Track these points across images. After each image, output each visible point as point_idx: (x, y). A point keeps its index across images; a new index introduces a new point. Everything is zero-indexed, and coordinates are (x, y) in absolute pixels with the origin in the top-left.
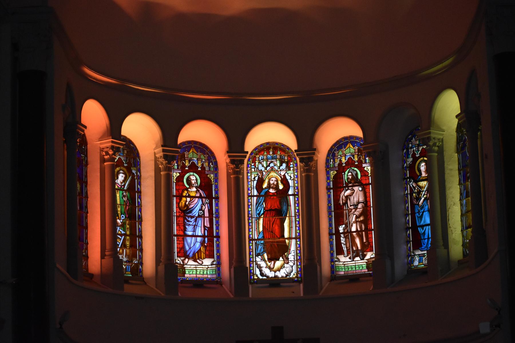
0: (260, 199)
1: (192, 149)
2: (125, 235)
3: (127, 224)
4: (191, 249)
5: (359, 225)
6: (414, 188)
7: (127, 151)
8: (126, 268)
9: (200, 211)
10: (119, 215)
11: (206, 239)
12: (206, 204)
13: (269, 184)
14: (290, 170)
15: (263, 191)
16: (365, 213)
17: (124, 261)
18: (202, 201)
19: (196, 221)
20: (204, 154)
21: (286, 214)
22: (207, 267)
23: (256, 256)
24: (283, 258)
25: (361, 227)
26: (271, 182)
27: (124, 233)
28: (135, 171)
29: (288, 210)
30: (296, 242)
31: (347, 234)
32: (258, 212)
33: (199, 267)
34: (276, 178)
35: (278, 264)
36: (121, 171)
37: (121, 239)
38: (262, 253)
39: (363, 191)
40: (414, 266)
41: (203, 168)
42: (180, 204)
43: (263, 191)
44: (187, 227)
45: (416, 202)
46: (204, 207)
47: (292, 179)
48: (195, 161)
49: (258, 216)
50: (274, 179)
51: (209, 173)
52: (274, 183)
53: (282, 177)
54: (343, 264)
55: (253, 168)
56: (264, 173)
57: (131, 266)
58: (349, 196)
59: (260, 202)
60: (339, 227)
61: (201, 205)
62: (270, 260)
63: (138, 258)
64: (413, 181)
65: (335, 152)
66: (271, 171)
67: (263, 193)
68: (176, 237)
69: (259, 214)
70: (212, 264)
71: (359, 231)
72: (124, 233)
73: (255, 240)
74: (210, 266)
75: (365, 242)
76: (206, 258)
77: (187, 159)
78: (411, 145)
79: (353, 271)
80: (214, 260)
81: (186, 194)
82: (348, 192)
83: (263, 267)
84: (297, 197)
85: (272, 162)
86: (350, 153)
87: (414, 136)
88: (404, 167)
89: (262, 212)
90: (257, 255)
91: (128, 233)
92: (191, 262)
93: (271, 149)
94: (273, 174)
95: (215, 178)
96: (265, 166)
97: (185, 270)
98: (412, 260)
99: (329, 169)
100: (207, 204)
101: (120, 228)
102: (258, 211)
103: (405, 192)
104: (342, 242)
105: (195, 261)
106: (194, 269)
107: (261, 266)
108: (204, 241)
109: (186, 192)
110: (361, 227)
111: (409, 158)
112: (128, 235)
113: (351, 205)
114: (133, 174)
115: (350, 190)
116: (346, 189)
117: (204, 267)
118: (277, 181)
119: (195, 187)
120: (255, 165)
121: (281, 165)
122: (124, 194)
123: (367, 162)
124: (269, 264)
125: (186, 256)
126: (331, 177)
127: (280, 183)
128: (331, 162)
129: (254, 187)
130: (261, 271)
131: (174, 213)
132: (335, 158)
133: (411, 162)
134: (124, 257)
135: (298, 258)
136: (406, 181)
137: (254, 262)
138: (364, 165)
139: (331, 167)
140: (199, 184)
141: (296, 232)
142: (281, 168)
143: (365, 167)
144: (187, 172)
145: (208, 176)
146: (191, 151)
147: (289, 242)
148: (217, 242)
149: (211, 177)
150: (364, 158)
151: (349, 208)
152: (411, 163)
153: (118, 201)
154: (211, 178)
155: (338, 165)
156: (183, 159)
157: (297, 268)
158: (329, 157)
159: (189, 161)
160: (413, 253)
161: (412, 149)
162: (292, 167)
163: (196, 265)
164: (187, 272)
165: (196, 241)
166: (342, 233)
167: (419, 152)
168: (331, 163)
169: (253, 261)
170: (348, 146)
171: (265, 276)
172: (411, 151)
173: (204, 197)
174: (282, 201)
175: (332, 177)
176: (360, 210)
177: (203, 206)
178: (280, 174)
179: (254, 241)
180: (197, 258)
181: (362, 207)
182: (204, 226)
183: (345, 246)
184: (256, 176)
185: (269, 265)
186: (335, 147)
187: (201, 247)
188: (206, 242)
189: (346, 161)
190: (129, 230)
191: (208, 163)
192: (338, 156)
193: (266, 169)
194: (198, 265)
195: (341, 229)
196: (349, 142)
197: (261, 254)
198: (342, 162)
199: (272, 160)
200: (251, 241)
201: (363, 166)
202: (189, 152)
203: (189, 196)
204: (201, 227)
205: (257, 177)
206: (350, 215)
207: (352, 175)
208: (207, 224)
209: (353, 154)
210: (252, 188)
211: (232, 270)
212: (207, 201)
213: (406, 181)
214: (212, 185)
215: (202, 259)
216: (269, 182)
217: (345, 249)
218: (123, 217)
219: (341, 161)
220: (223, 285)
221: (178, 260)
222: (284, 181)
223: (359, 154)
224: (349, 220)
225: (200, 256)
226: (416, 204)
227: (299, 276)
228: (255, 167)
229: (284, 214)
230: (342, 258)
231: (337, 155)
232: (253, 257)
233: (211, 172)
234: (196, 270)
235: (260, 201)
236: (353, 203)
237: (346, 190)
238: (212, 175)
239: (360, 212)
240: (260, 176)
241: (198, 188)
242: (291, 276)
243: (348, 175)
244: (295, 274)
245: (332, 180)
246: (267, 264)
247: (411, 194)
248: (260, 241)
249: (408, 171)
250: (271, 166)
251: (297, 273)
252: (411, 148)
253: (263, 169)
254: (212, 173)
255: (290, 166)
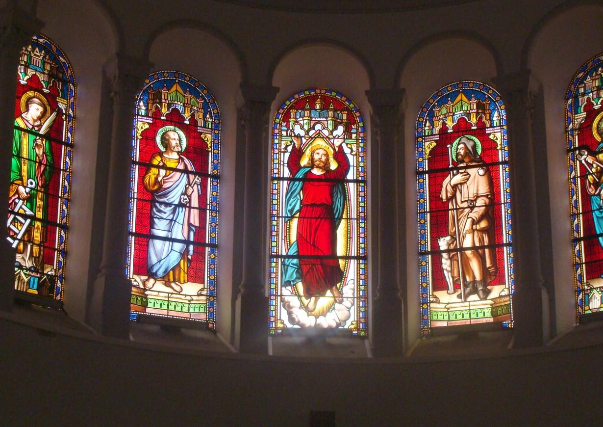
0: (294, 185)
1: (175, 86)
2: (33, 218)
3: (39, 199)
4: (162, 262)
5: (478, 236)
6: (591, 165)
7: (51, 67)
8: (29, 282)
9: (182, 196)
10: (25, 179)
11: (191, 248)
12: (196, 185)
13: (312, 160)
14: (351, 138)
15: (301, 170)
16: (492, 212)
17: (26, 267)
18: (188, 178)
19: (174, 212)
20: (196, 97)
21: (341, 213)
22: (189, 298)
23: (282, 286)
24: (332, 292)
25: (481, 240)
26: (316, 157)
27: (31, 213)
28: (64, 106)
29: (346, 206)
30: (359, 264)
31: (455, 253)
32: (290, 208)
33: (173, 298)
34: (325, 150)
35: (325, 300)
36: (36, 100)
37: (23, 224)
38: (293, 281)
39: (486, 176)
40: (590, 309)
41: (193, 119)
42: (147, 180)
43: (300, 171)
44: (156, 220)
45: (594, 191)
46: (190, 190)
47: (354, 153)
48: (179, 106)
49: (289, 215)
50: (321, 152)
51: (204, 132)
52: (321, 158)
53: (337, 149)
54: (445, 308)
55: (284, 130)
56: (304, 141)
57: (40, 278)
58: (459, 186)
59: (293, 189)
60: (439, 239)
61: (186, 185)
62: (309, 293)
63: (56, 266)
64: (586, 153)
65: (434, 110)
66: (317, 137)
67: (300, 175)
68: (133, 238)
69: (291, 211)
70: (199, 295)
71: (479, 248)
72: (31, 213)
73: (282, 256)
74: (194, 298)
75: (490, 268)
76: (188, 281)
77: (164, 102)
78: (583, 89)
79: (465, 321)
80: (204, 288)
81: (160, 162)
82: (458, 179)
83: (295, 307)
84: (363, 185)
85: (319, 122)
86: (462, 110)
87: (589, 73)
88: (569, 130)
89: (297, 208)
90: (288, 283)
91: (39, 215)
92: (160, 286)
93: (319, 100)
94: (319, 142)
95: (214, 142)
96: (306, 127)
97: (147, 299)
98: (585, 298)
99: (423, 139)
100: (198, 185)
101: (23, 204)
102: (290, 205)
103: (571, 174)
104: (444, 266)
105: (167, 284)
106: (165, 300)
107: (291, 304)
108: (187, 250)
109: (159, 158)
110: (481, 240)
111: (579, 112)
112: (39, 220)
113: (462, 200)
114: (60, 110)
115: (461, 175)
116: (453, 173)
117: (183, 297)
118: (327, 155)
119: (176, 152)
120: (288, 126)
121: (335, 128)
122: (39, 142)
123: (495, 125)
124: (306, 301)
125: (152, 275)
126: (425, 153)
127: (331, 159)
128: (425, 126)
129: (284, 163)
130: (290, 314)
131: (134, 193)
132: (434, 119)
133: (582, 120)
134: (27, 259)
135: (361, 294)
136: (573, 154)
137: (279, 298)
138: (488, 131)
139: (427, 134)
140: (184, 148)
141: (358, 247)
142: (335, 133)
143: (490, 134)
144: (165, 123)
145: (203, 136)
146: (174, 88)
147: (346, 263)
148: (210, 254)
149: (206, 139)
150: (488, 118)
151: (459, 206)
152: (583, 121)
153: (25, 153)
154: (208, 140)
155: (439, 132)
156: (158, 101)
157: (359, 311)
158: (423, 119)
159: (169, 105)
160: (587, 285)
161: (586, 97)
162: (354, 133)
163: (169, 293)
164: (150, 305)
165: (172, 249)
166: (444, 251)
167: (600, 101)
168: (427, 128)
169: (276, 296)
170: (459, 98)
171: (298, 323)
172: (583, 101)
173: (192, 173)
174: (334, 190)
175: (428, 152)
176: (480, 210)
177: (190, 187)
178: (333, 144)
179: (280, 259)
180: (171, 279)
181: (484, 205)
182: (190, 224)
183: (450, 274)
184: (289, 145)
185: (306, 304)
186: (434, 101)
187: (180, 261)
188: (191, 252)
189: (455, 124)
190: (41, 210)
191: (203, 113)
192: (439, 116)
193: (307, 132)
194: (172, 293)
195: (443, 243)
196: (461, 92)
197: (292, 283)
198: (447, 126)
199: (319, 119)
200: (275, 259)
201: (487, 132)
202: (169, 90)
203: (164, 167)
204: (183, 225)
205: (292, 146)
206: (460, 219)
207: (466, 147)
208: (195, 221)
209: (468, 112)
210: (281, 165)
211: (239, 303)
212: (198, 179)
213: (573, 154)
214: (208, 152)
215: (180, 283)
216: (312, 156)
217: (450, 281)
218: (31, 183)
219: (444, 124)
220: (218, 334)
221: (136, 281)
222: (340, 156)
223: (480, 111)
224: (458, 227)
225: (177, 277)
226: (594, 195)
227: (361, 328)
228: (288, 128)
229: (337, 214)
230: (442, 295)
231: (438, 113)
232: (276, 288)
233: (207, 129)
234: (168, 301)
235: (295, 188)
236: (466, 198)
237: (454, 175)
238: (210, 136)
239: (480, 213)
240: (296, 146)
241: (181, 154)
242: (346, 327)
243: (457, 149)
244: (355, 323)
245: (427, 157)
246: (301, 302)
247: (584, 177)
248: (291, 259)
249: (577, 137)
250: (316, 129)
251: (358, 322)
252: (583, 95)
253: (302, 133)
254: (208, 132)
255: (352, 132)
